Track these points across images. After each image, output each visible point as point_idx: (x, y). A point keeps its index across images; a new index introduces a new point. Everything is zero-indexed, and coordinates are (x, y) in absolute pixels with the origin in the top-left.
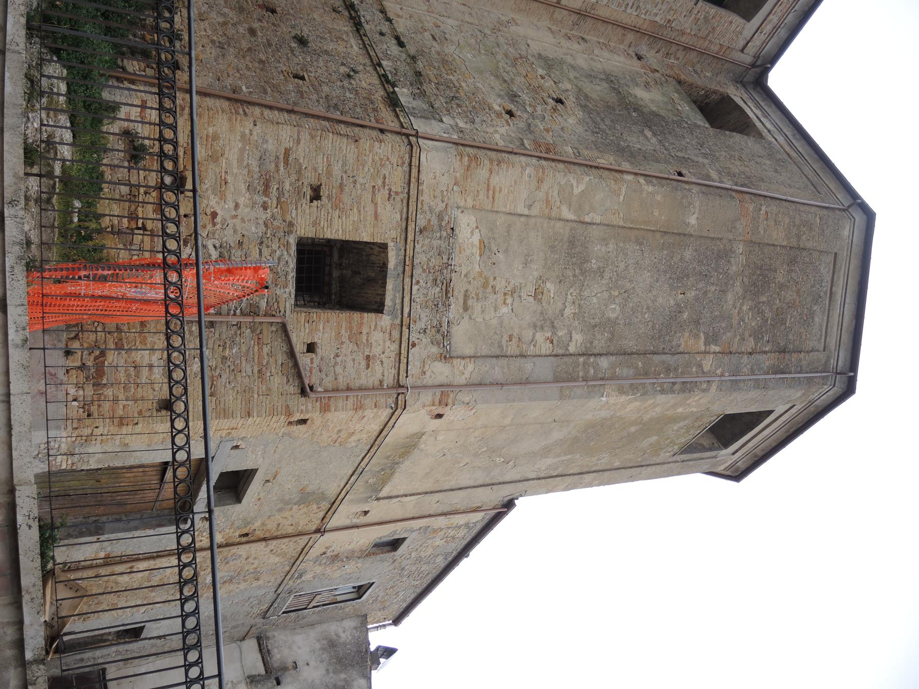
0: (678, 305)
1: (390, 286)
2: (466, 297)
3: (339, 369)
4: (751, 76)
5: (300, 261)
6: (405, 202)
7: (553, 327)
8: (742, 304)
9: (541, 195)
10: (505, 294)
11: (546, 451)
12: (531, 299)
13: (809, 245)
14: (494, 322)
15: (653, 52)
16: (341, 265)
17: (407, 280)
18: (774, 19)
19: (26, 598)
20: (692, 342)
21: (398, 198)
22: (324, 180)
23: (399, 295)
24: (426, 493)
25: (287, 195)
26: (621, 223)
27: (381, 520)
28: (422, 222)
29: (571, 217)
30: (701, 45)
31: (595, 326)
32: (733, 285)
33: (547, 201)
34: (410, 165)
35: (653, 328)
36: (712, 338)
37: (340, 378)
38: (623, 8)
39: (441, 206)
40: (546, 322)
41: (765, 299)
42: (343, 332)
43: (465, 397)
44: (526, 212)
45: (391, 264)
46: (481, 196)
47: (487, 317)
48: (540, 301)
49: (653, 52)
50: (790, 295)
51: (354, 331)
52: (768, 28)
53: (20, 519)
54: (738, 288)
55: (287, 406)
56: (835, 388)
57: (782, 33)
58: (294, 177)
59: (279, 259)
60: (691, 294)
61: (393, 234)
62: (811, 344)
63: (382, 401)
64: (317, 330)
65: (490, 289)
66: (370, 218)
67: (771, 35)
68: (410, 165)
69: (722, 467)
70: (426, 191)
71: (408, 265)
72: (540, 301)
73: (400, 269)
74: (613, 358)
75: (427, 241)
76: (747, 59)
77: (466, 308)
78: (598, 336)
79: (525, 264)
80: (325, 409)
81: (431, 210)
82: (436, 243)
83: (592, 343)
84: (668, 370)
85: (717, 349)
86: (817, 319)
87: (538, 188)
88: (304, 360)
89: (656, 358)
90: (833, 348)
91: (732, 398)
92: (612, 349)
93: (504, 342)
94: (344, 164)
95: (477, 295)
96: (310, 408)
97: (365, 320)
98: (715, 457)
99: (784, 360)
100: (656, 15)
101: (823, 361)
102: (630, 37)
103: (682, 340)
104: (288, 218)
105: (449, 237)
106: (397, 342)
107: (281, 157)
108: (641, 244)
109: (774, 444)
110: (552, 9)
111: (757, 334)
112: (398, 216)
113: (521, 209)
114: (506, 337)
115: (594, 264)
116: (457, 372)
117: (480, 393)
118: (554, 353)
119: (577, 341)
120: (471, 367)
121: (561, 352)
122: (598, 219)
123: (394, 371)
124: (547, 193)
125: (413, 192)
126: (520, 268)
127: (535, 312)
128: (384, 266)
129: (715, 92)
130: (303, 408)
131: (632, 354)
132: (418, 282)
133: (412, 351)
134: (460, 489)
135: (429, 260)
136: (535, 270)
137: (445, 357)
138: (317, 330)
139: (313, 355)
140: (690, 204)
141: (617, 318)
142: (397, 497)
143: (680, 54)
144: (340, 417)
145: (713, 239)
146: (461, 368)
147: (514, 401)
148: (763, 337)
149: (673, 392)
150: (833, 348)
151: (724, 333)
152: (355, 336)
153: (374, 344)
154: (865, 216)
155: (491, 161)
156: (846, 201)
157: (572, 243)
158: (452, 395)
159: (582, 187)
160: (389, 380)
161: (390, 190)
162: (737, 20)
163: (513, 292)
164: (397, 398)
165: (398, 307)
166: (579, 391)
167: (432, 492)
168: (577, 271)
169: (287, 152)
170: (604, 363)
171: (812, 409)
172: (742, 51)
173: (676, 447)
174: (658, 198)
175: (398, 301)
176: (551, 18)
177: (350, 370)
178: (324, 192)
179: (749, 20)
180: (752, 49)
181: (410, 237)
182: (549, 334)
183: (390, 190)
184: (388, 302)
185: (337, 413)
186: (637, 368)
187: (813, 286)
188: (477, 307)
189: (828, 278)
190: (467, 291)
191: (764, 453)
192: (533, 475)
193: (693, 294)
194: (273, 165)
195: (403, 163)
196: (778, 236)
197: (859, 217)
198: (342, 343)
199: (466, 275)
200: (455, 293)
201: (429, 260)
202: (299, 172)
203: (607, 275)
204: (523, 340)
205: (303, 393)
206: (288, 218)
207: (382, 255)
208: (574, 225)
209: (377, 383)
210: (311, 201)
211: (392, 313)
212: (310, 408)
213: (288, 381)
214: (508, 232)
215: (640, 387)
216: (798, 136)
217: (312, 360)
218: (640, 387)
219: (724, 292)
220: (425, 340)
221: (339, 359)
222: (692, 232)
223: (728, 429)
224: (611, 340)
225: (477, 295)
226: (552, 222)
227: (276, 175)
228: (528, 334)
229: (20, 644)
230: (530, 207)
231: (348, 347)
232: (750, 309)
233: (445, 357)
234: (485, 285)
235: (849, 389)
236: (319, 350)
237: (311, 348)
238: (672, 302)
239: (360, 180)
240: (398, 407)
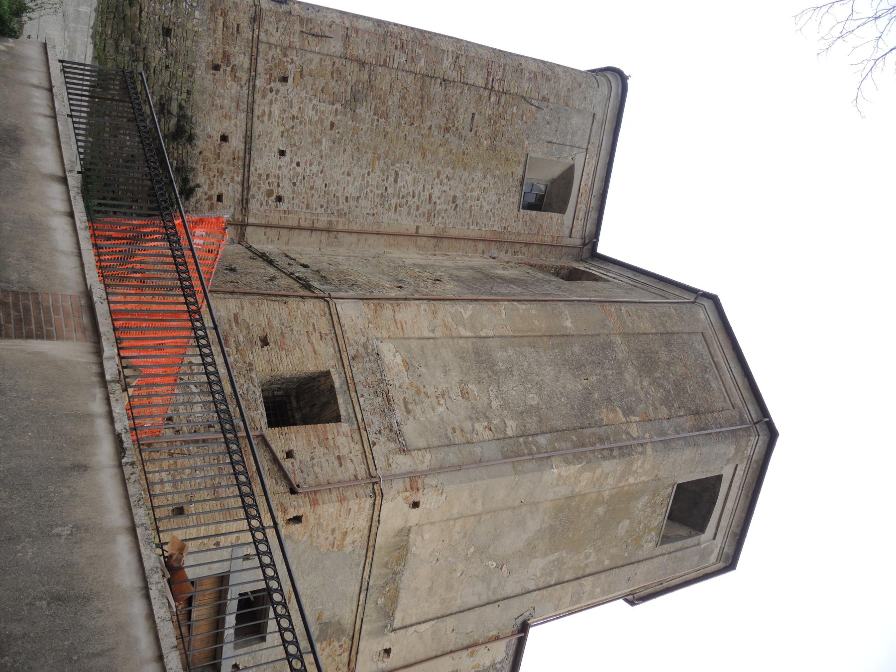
0: (587, 388)
1: (340, 400)
2: (405, 403)
3: (317, 470)
4: (586, 253)
5: (267, 409)
6: (334, 339)
7: (487, 417)
8: (641, 381)
9: (438, 321)
10: (437, 397)
11: (530, 550)
12: (461, 398)
13: (675, 329)
14: (436, 419)
15: (503, 253)
16: (300, 408)
17: (353, 394)
18: (582, 207)
19: (103, 338)
20: (611, 416)
21: (328, 338)
22: (268, 331)
23: (350, 407)
24: (438, 618)
25: (242, 345)
26: (511, 334)
27: (406, 663)
28: (352, 352)
29: (469, 334)
30: (538, 239)
31: (522, 413)
32: (626, 367)
33: (446, 326)
34: (331, 314)
35: (573, 408)
36: (629, 411)
37: (320, 476)
38: (466, 227)
39: (364, 339)
40: (477, 415)
41: (659, 375)
42: (312, 439)
43: (431, 481)
44: (432, 335)
45: (337, 384)
46: (392, 329)
47: (428, 416)
48: (468, 399)
49: (503, 253)
50: (680, 369)
51: (322, 438)
52: (581, 215)
53: (95, 299)
54: (631, 369)
55: (281, 504)
56: (761, 437)
57: (593, 215)
58: (245, 332)
59: (247, 390)
60: (593, 379)
61: (332, 363)
62: (720, 405)
63: (361, 492)
64: (291, 440)
65: (423, 395)
66: (311, 354)
67: (586, 219)
68: (331, 314)
69: (713, 558)
70: (348, 330)
71: (350, 383)
72: (468, 399)
73: (345, 387)
74: (549, 435)
75: (360, 365)
76: (577, 241)
77: (408, 412)
78: (529, 420)
79: (446, 372)
80: (314, 503)
81: (357, 343)
82: (368, 365)
83: (525, 426)
84: (601, 440)
85: (637, 419)
86: (713, 385)
87: (435, 317)
88: (287, 464)
89: (587, 431)
90: (741, 405)
91: (672, 460)
92: (544, 429)
93: (450, 434)
94: (280, 320)
95: (414, 400)
96: (301, 503)
97: (328, 429)
98: (699, 544)
99: (702, 423)
100: (493, 226)
101: (737, 416)
102: (481, 246)
103: (603, 416)
104: (248, 361)
105: (376, 360)
106: (360, 443)
107: (233, 319)
108: (534, 347)
109: (744, 515)
110: (414, 238)
111: (667, 402)
112: (332, 350)
113: (427, 334)
114: (450, 431)
115: (502, 366)
116: (418, 462)
117: (442, 478)
118: (496, 437)
119: (512, 427)
120: (428, 456)
121: (501, 436)
122: (491, 333)
123: (364, 467)
124: (443, 320)
125: (339, 332)
126: (442, 376)
127: (467, 408)
128: (332, 389)
129: (562, 268)
130: (295, 503)
131: (563, 430)
132: (362, 396)
133: (374, 449)
134: (469, 609)
135: (366, 378)
136: (455, 375)
137: (404, 451)
138: (291, 440)
139: (293, 460)
140: (561, 313)
141: (538, 404)
142: (412, 625)
143: (524, 250)
144: (328, 509)
145: (592, 336)
146: (420, 458)
147: (476, 480)
148: (673, 405)
149: (614, 457)
150: (741, 405)
151: (637, 405)
152: (323, 442)
153: (341, 447)
154: (710, 301)
155: (392, 305)
156: (691, 297)
157: (477, 353)
158: (420, 481)
159: (469, 313)
160: (362, 473)
161: (320, 333)
162: (556, 216)
163: (443, 395)
164: (373, 488)
165: (352, 415)
166: (530, 465)
167: (443, 617)
168: (490, 373)
169: (236, 316)
170: (542, 440)
171: (754, 465)
172: (570, 237)
173: (653, 533)
174: (534, 312)
175: (351, 411)
176: (416, 246)
177: (326, 469)
178: (270, 339)
179: (564, 213)
180: (577, 233)
181: (346, 363)
182: (486, 424)
183: (320, 333)
184: (343, 413)
185: (325, 506)
186: (572, 441)
187: (696, 360)
188: (418, 410)
189: (706, 352)
190: (404, 398)
191: (740, 528)
192: (534, 588)
193: (595, 378)
194: (227, 326)
195: (325, 314)
196: (645, 326)
197: (707, 303)
198: (314, 448)
199: (400, 387)
200: (396, 401)
201: (366, 378)
202: (248, 328)
203: (515, 373)
204: (465, 430)
205: (293, 491)
206: (248, 361)
207: (329, 380)
208: (474, 340)
209: (352, 477)
210: (262, 347)
211: (349, 420)
212: (301, 503)
213: (277, 483)
214: (423, 351)
215: (583, 456)
216: (637, 274)
217: (292, 463)
218: (583, 456)
219: (621, 373)
220: (383, 439)
221: (315, 461)
222: (572, 333)
223: (692, 506)
224: (540, 422)
225: (414, 400)
226: (456, 340)
227: (231, 332)
228: (468, 426)
229: (102, 375)
230: (433, 331)
231: (320, 451)
232: (650, 384)
233: (404, 451)
234: (418, 392)
235: (772, 434)
236: (296, 456)
237: (289, 455)
238: (580, 387)
239: (296, 328)
240: (377, 496)
